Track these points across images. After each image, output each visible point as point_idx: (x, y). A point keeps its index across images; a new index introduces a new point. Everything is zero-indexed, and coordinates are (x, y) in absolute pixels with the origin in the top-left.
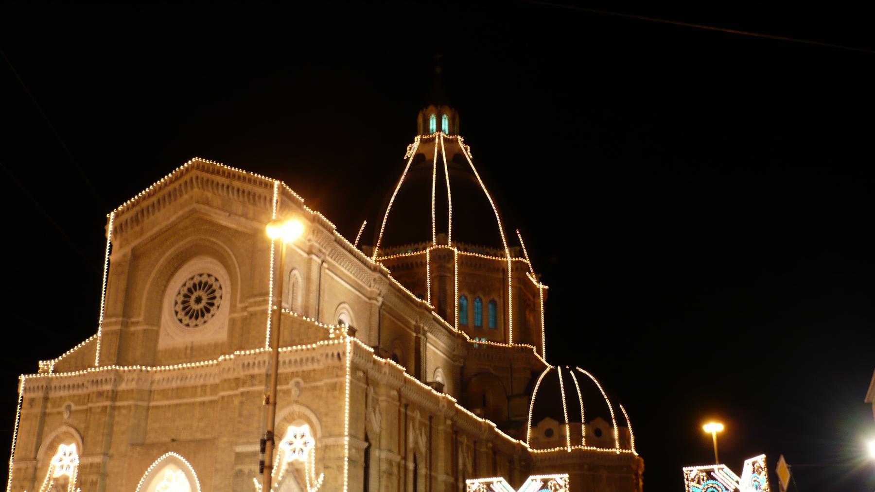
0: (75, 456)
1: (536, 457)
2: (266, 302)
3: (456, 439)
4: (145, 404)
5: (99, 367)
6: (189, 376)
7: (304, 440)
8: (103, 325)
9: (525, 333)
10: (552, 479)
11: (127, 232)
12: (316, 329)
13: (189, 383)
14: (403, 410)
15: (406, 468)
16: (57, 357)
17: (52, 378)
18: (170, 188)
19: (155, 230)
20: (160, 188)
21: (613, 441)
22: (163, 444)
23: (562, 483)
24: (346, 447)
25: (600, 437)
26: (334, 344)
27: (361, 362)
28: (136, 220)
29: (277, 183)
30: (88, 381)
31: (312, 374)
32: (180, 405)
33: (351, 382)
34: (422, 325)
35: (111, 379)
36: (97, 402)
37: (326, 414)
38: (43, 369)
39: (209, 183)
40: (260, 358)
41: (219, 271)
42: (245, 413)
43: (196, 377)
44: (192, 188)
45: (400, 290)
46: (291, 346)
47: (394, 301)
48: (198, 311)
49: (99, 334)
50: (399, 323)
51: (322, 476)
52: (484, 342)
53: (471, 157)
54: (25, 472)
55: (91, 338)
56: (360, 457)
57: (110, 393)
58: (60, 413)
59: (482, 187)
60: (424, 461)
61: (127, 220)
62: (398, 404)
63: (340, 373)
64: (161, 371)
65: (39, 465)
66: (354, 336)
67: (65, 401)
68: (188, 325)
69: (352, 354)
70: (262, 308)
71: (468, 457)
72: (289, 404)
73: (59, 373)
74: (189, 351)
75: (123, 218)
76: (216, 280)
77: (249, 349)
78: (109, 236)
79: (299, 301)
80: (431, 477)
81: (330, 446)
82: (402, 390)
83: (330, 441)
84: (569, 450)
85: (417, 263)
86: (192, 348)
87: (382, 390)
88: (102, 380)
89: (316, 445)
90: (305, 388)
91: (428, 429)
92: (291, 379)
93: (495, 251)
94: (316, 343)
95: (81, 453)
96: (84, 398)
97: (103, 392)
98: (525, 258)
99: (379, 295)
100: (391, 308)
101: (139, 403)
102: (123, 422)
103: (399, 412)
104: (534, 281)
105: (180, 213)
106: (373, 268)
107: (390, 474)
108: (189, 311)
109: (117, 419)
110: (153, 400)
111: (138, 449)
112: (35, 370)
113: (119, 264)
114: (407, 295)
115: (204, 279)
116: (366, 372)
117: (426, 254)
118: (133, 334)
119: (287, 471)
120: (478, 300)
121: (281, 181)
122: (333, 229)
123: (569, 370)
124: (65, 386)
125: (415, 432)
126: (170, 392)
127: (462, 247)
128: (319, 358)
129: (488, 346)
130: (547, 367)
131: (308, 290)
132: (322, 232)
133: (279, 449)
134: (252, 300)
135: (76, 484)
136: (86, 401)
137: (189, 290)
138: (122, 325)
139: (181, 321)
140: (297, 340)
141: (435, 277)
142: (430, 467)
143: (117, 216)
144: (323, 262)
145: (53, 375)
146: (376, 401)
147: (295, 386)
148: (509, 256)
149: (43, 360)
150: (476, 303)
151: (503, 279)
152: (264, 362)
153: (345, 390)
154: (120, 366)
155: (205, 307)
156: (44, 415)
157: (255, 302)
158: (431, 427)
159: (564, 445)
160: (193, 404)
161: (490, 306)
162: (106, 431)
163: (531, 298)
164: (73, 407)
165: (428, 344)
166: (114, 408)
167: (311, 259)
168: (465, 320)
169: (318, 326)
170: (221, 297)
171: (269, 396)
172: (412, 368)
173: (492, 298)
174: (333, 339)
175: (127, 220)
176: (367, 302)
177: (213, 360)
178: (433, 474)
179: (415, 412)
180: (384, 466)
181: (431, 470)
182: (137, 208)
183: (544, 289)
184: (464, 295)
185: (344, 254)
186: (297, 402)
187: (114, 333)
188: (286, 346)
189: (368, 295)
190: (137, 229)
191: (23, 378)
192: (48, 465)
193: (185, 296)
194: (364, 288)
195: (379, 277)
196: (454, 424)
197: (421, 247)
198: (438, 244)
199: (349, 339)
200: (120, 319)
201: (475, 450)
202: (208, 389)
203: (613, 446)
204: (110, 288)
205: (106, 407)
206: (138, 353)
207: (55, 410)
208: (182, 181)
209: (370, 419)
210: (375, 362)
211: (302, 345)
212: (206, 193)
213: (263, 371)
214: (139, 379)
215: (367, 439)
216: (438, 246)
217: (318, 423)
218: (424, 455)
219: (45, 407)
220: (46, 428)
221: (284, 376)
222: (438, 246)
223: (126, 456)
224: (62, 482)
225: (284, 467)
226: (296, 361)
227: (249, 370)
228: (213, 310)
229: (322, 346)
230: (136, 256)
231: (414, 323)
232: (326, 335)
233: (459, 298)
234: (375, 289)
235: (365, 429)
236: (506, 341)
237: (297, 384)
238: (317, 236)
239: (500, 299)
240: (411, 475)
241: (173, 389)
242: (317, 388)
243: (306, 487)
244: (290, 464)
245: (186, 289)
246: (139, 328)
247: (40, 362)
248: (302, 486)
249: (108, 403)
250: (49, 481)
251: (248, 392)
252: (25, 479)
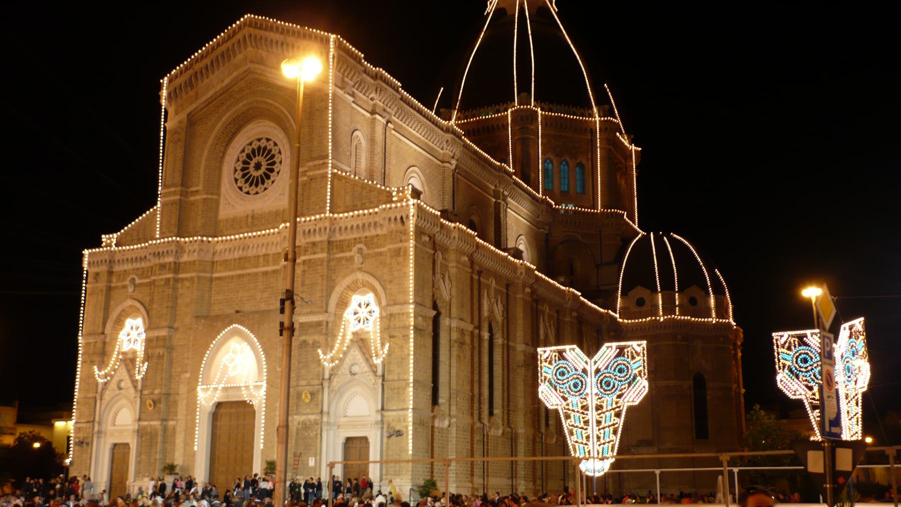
0: (142, 329)
1: (626, 327)
2: (325, 165)
3: (537, 307)
4: (208, 275)
5: (159, 239)
6: (251, 246)
7: (369, 309)
8: (164, 195)
9: (615, 197)
10: (629, 346)
11: (181, 98)
12: (378, 192)
13: (251, 253)
14: (476, 277)
15: (480, 338)
16: (119, 231)
17: (115, 252)
18: (223, 48)
19: (211, 93)
20: (213, 48)
21: (709, 309)
22: (228, 316)
23: (639, 349)
24: (412, 315)
25: (695, 306)
26: (396, 207)
27: (427, 226)
28: (190, 84)
29: (333, 37)
30: (150, 254)
31: (375, 240)
32: (242, 276)
33: (416, 247)
34: (502, 190)
35: (172, 251)
36: (160, 274)
37: (391, 282)
38: (106, 242)
39: (263, 40)
40: (321, 225)
41: (278, 135)
42: (307, 282)
43: (258, 246)
44: (246, 48)
45: (475, 152)
46: (353, 211)
47: (470, 165)
48: (258, 177)
49: (159, 205)
50: (476, 188)
51: (387, 345)
52: (571, 207)
53: (557, 10)
54: (94, 346)
55: (151, 210)
56: (428, 325)
57: (172, 265)
58: (125, 287)
59: (568, 42)
60: (500, 332)
61: (181, 85)
62: (470, 270)
63: (403, 238)
64: (222, 241)
65: (108, 340)
66: (419, 198)
67: (129, 274)
68: (248, 193)
69: (415, 218)
70: (322, 171)
71: (550, 326)
72: (353, 271)
73: (121, 246)
74: (250, 220)
75: (178, 82)
76: (275, 144)
77: (309, 215)
78: (163, 102)
79: (363, 164)
80: (508, 347)
81: (396, 314)
82: (475, 255)
83: (395, 309)
84: (662, 319)
85: (498, 125)
86: (253, 217)
87: (452, 256)
88: (163, 252)
89: (381, 314)
90: (369, 254)
91: (505, 297)
92: (354, 246)
93: (582, 110)
94: (378, 207)
95: (147, 326)
96: (148, 271)
97: (166, 263)
98: (616, 118)
99: (453, 157)
100: (466, 171)
101: (202, 274)
102: (187, 295)
103: (472, 278)
104: (626, 143)
105: (235, 74)
106: (445, 128)
107: (462, 344)
109: (180, 291)
110: (216, 272)
111: (203, 321)
112: (98, 244)
113: (175, 132)
114: (485, 157)
115: (263, 143)
116: (432, 236)
117: (507, 115)
118: (193, 204)
119: (352, 341)
120: (564, 163)
121: (337, 34)
122: (398, 87)
123: (662, 236)
124: (128, 259)
125: (490, 301)
126: (233, 262)
127: (546, 107)
128: (381, 222)
129: (575, 212)
131: (372, 152)
132: (386, 89)
133: (344, 319)
134: (311, 164)
135: (144, 358)
136: (150, 274)
137: (248, 156)
138: (181, 195)
139: (241, 188)
140: (359, 204)
141: (517, 140)
142: (508, 336)
143: (170, 81)
144: (388, 122)
145: (116, 248)
146: (445, 268)
147: (358, 253)
148: (597, 115)
149: (105, 234)
150: (562, 166)
151: (591, 139)
152: (325, 228)
153: (410, 255)
154: (180, 237)
155: (265, 173)
156: (109, 289)
157: (315, 166)
158: (508, 296)
159: (657, 314)
160: (256, 274)
161: (578, 169)
162: (170, 304)
163: (623, 161)
164: (138, 281)
165: (509, 210)
166: (177, 280)
167: (375, 119)
168: (550, 185)
169: (380, 189)
170: (281, 162)
171: (288, 251)
172: (492, 235)
173: (578, 161)
174: (396, 202)
175: (181, 85)
176: (440, 166)
177: (273, 228)
178: (511, 344)
179: (490, 280)
180: (455, 336)
181: (508, 340)
182: (190, 72)
183: (635, 151)
184: (549, 158)
185: (411, 114)
186: (360, 269)
187: (173, 203)
188: (347, 212)
189: (440, 158)
190: (192, 93)
191: (86, 252)
192: (116, 339)
193: (245, 162)
194: (436, 151)
195: (452, 138)
196: (533, 292)
197: (502, 108)
198: (520, 104)
199: (412, 201)
200: (179, 188)
201: (558, 319)
202: (270, 259)
203: (710, 316)
204: (167, 156)
205: (169, 279)
206: (200, 222)
207: (119, 284)
208: (234, 40)
209: (439, 286)
210: (442, 225)
211: (363, 209)
213: (325, 238)
214: (201, 250)
215: (435, 307)
216: (520, 106)
217: (382, 290)
218: (500, 324)
219: (110, 281)
220: (112, 303)
221: (347, 242)
222: (520, 106)
223: (191, 329)
224: (130, 356)
225: (349, 337)
226: (358, 226)
227: (310, 237)
228: (273, 176)
229: (384, 209)
230: (192, 122)
231: (493, 188)
232: (389, 199)
233: (544, 162)
234: (447, 151)
235: (433, 296)
236: (594, 206)
237: (360, 251)
238: (380, 94)
239: (588, 161)
240: (486, 345)
241: (235, 259)
242: (380, 254)
243: (371, 357)
244: (354, 334)
245: (244, 154)
246: (198, 197)
247: (103, 236)
248: (367, 356)
249: (170, 276)
250: (118, 355)
251: (310, 260)
252: (94, 353)
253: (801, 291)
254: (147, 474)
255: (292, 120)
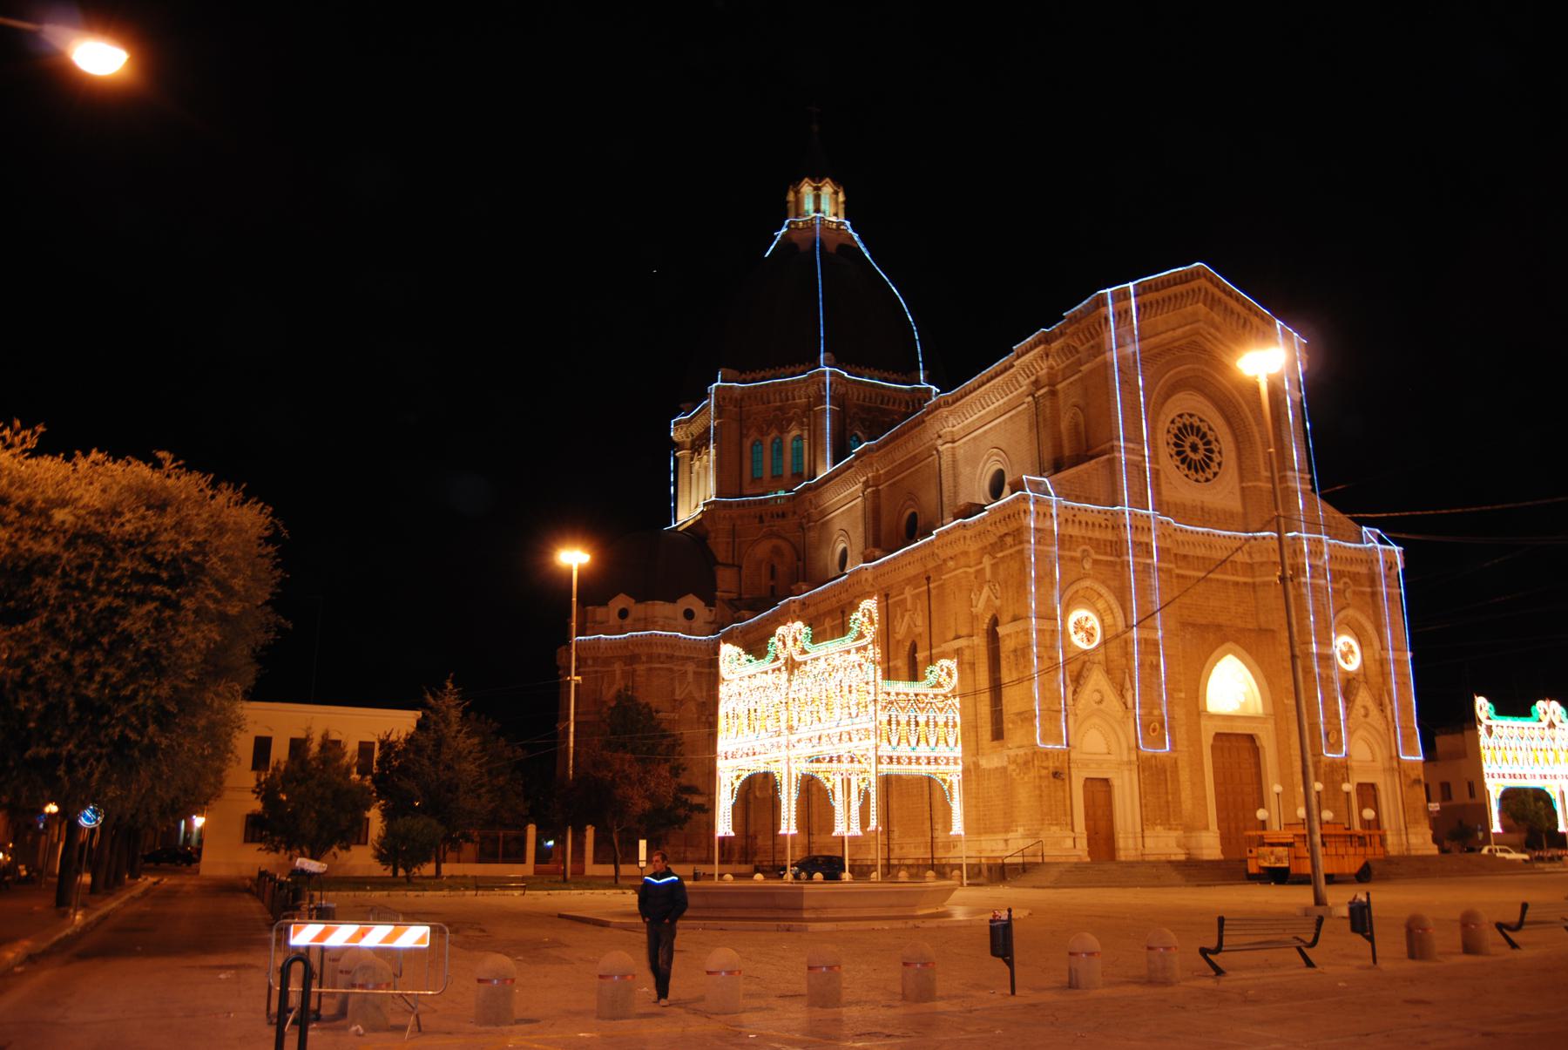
108: (1186, 430)
120: (854, 438)
130: (523, 861)
137: (1208, 443)
193: (1204, 435)
212: (1213, 314)
253: (552, 555)
254: (1159, 821)
255: (1153, 400)
